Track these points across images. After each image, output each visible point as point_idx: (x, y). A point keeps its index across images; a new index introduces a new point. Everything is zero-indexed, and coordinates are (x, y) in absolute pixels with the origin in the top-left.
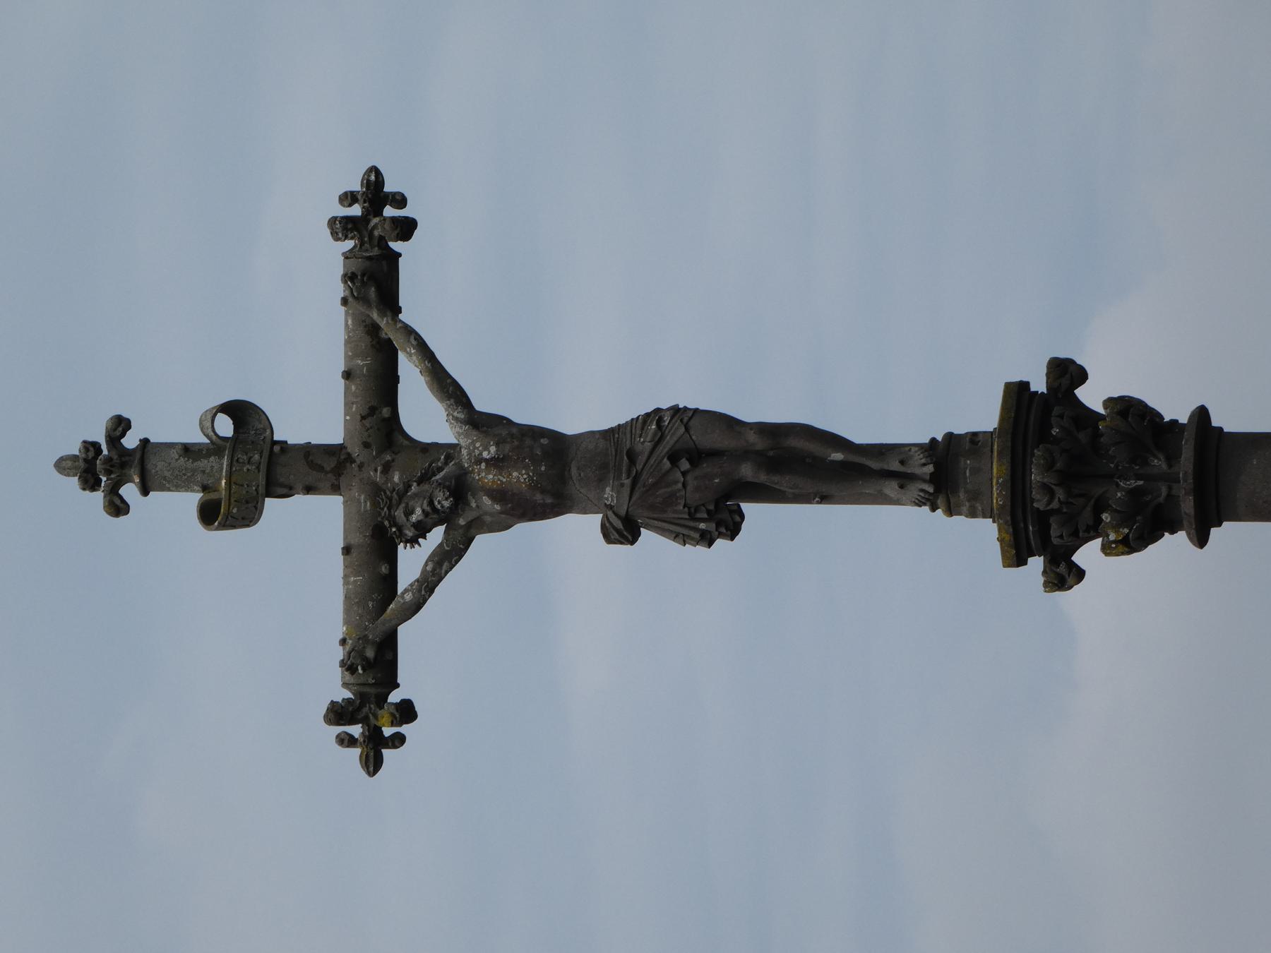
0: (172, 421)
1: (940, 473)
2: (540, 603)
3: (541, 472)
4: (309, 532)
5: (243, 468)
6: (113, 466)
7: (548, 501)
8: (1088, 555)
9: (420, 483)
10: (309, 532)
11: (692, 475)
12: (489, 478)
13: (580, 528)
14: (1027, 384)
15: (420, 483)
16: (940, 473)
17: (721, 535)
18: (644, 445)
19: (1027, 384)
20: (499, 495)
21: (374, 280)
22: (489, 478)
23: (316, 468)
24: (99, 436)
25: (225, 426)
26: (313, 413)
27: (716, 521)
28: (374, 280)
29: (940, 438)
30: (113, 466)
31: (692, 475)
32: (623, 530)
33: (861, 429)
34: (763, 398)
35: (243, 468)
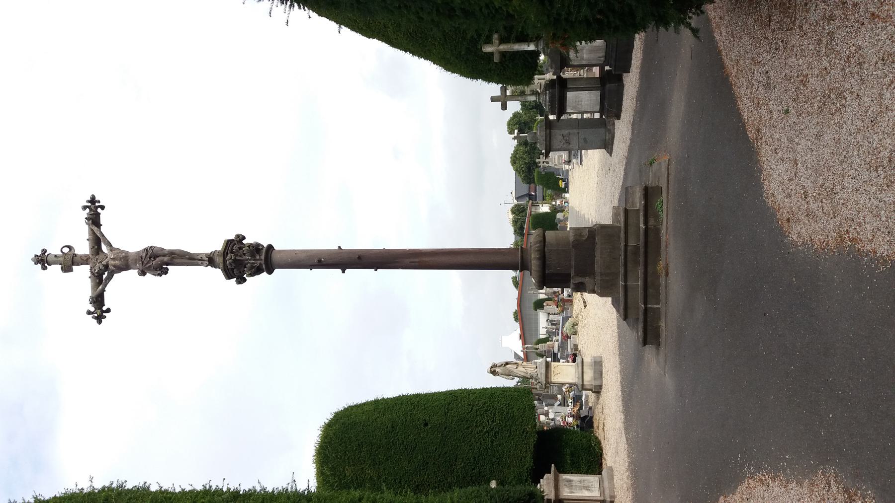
0: (54, 250)
1: (210, 260)
2: (124, 287)
3: (124, 263)
4: (83, 273)
5: (69, 261)
6: (43, 260)
7: (125, 267)
8: (32, 501)
9: (104, 264)
10: (83, 273)
11: (155, 262)
12: (112, 262)
13: (133, 273)
14: (240, 238)
15: (104, 264)
16: (210, 260)
17: (523, 143)
18: (144, 255)
19: (240, 238)
20: (114, 266)
21: (94, 220)
22: (112, 262)
23: (84, 260)
24: (39, 253)
25: (66, 250)
26: (83, 248)
27: (161, 271)
28: (94, 220)
29: (616, 122)
30: (43, 260)
31: (155, 262)
32: (143, 273)
33: (192, 249)
34: (169, 244)
35: (69, 261)
